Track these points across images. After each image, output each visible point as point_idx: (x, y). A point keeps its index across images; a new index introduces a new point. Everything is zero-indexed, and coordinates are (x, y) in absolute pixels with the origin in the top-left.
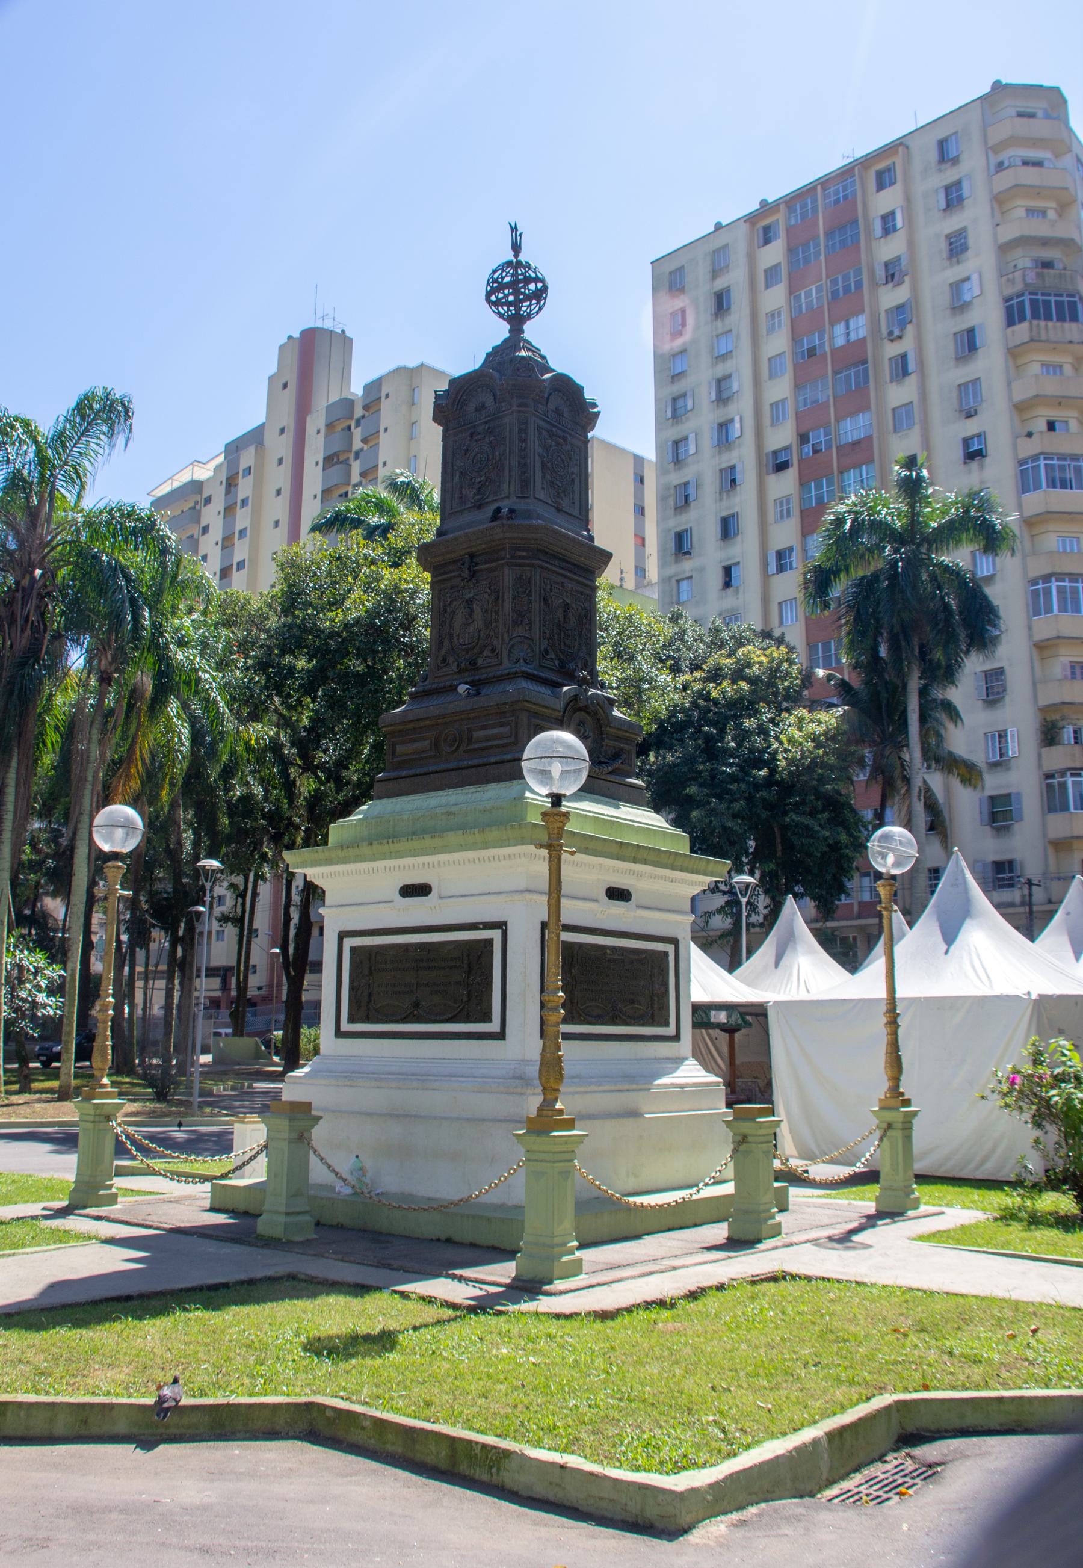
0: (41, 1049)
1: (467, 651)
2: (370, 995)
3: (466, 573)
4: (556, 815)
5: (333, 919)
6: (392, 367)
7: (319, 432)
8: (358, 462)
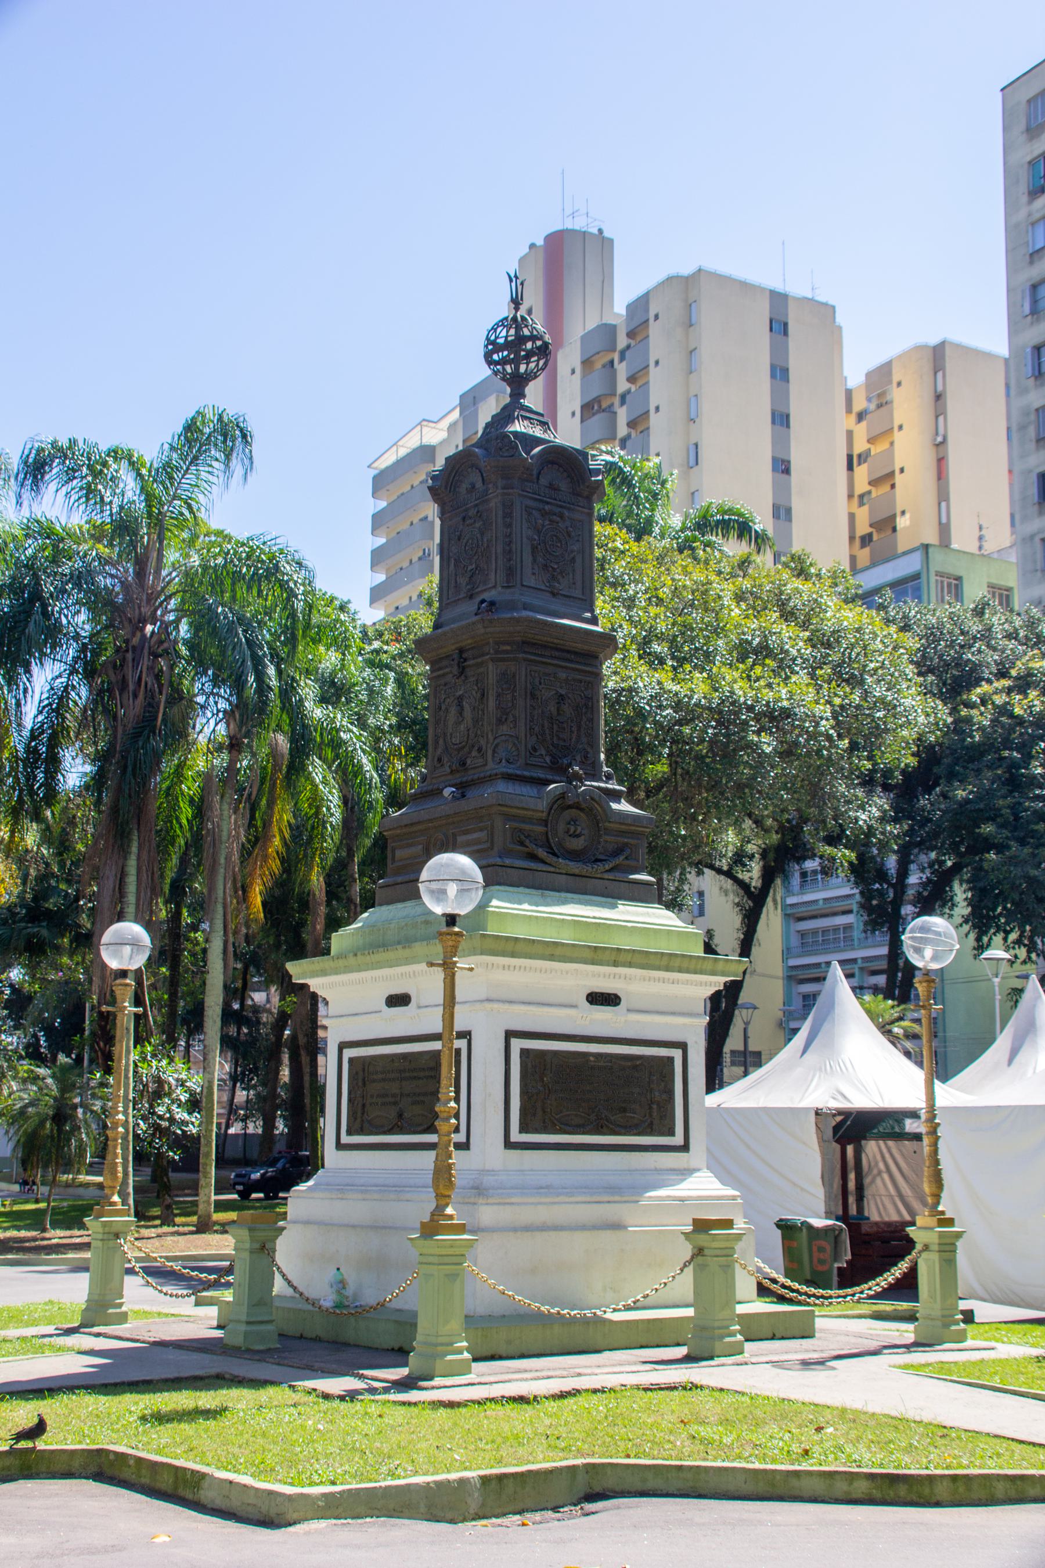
0: (237, 1176)
1: (459, 750)
2: (364, 1105)
3: (455, 670)
4: (448, 934)
5: (335, 1030)
6: (661, 277)
7: (573, 372)
8: (625, 408)
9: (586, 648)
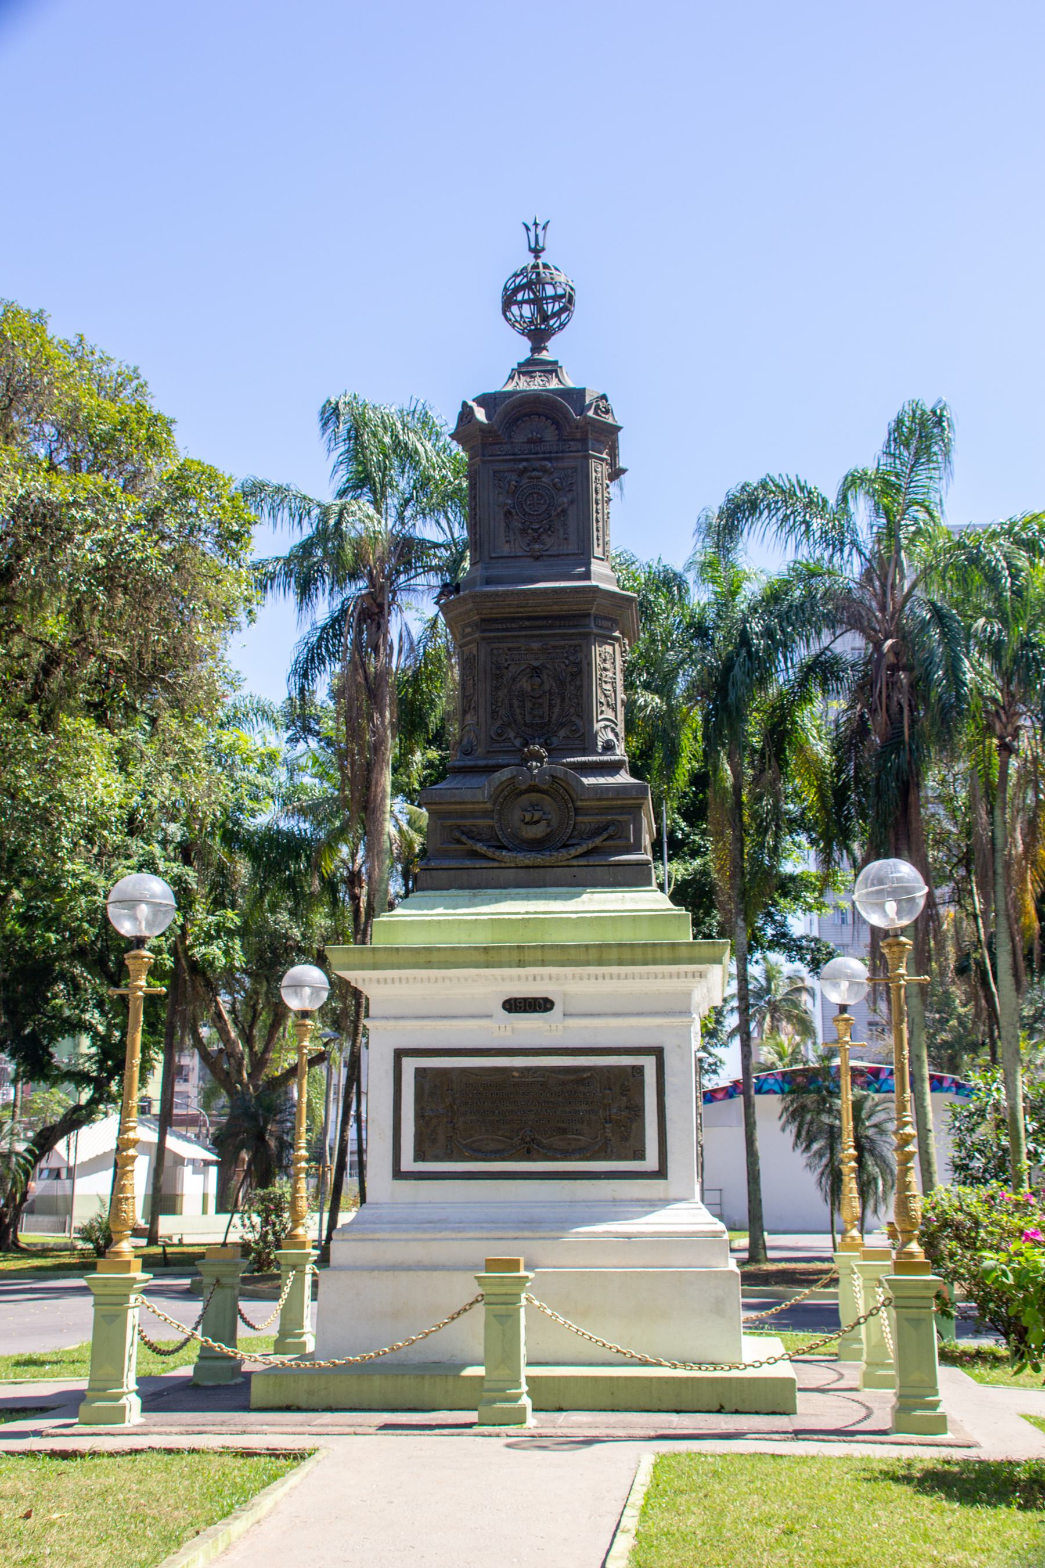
9: (566, 608)
